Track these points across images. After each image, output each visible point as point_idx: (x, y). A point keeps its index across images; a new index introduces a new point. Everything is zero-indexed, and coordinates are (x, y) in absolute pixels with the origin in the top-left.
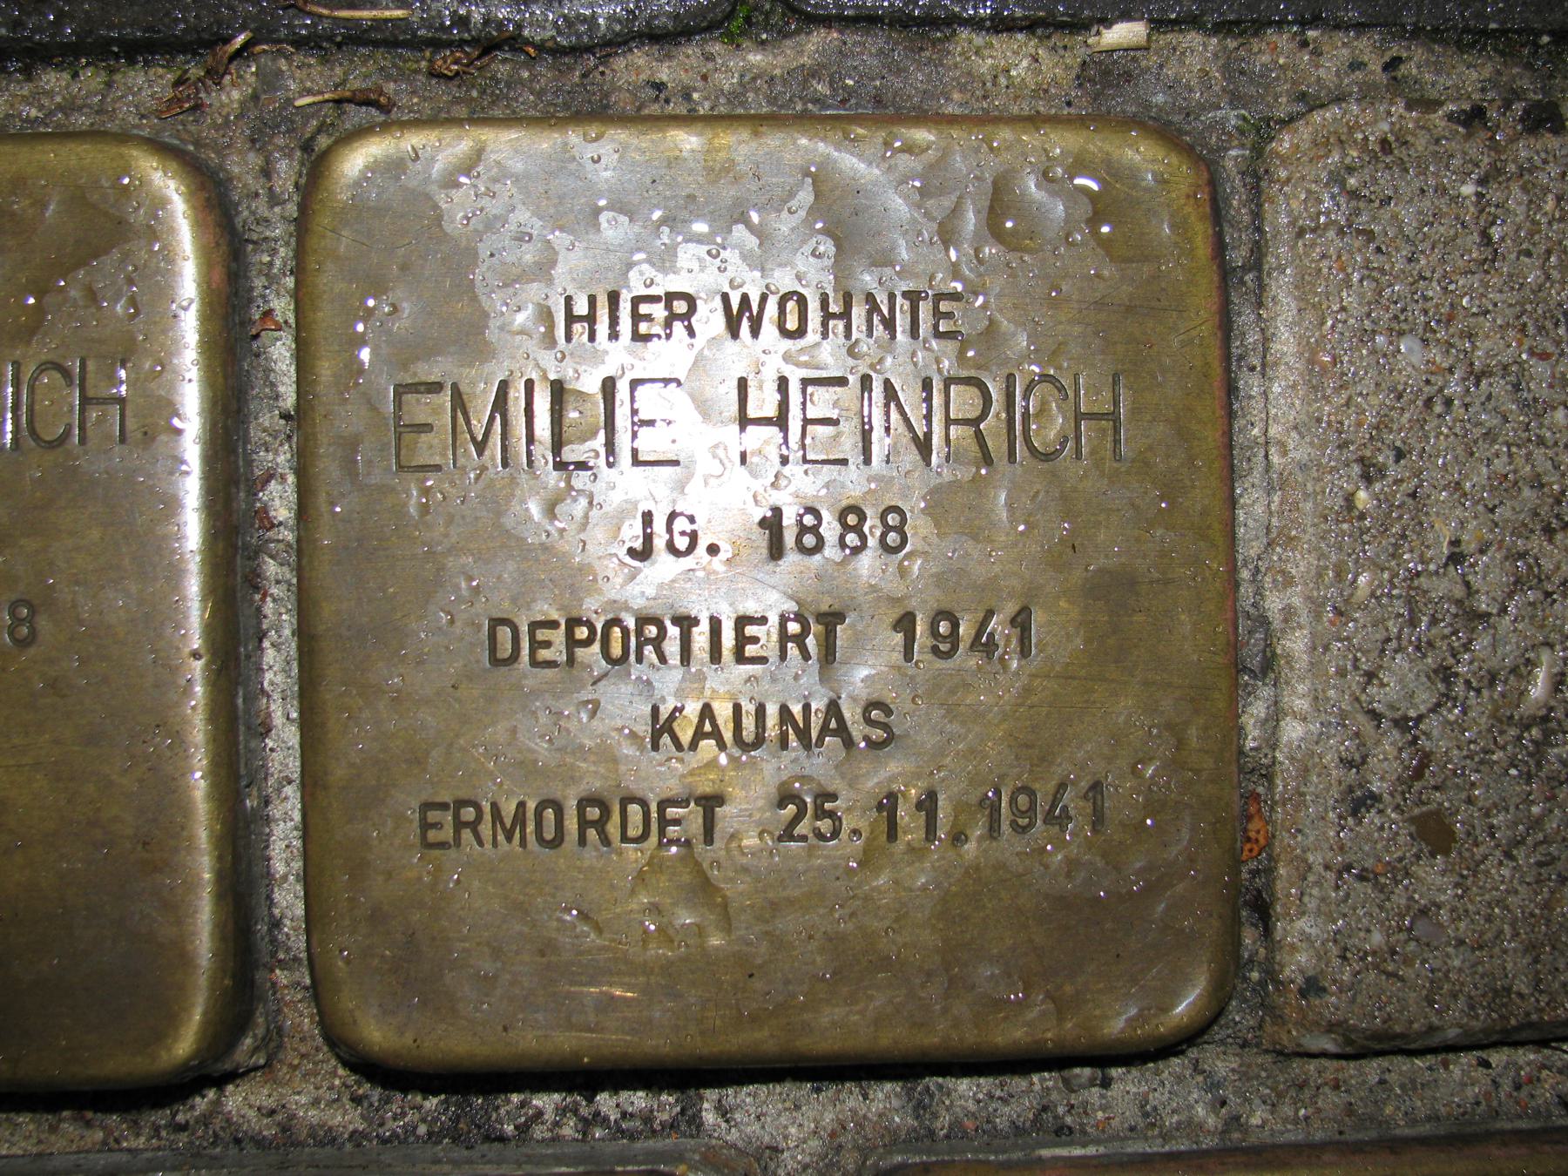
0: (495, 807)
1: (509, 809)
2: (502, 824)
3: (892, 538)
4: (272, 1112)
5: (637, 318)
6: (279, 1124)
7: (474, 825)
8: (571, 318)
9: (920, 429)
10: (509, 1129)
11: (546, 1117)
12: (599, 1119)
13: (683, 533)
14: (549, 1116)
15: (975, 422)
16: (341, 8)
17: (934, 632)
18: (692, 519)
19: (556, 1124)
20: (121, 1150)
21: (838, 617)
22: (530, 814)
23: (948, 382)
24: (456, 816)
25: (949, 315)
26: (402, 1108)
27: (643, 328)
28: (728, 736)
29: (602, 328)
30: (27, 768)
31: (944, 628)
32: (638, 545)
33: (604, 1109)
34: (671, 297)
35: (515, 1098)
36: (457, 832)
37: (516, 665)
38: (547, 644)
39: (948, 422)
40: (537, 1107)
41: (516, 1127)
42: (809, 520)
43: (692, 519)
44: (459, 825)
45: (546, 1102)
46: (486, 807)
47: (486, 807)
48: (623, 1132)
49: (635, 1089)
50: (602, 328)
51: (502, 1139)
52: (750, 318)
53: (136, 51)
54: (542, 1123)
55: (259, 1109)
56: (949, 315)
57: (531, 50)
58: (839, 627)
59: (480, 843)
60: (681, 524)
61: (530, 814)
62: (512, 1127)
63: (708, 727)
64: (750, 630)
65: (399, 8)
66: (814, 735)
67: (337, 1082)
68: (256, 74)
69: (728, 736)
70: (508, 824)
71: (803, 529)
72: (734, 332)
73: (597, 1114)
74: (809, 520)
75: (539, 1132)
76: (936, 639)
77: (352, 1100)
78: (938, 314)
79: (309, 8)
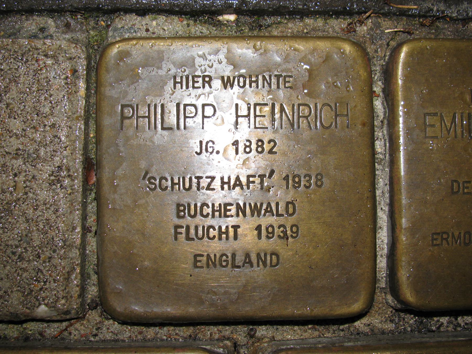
0: (453, 233)
1: (456, 234)
2: (455, 238)
3: (260, 149)
4: (369, 325)
5: (194, 82)
6: (370, 328)
7: (446, 239)
8: (175, 83)
9: (290, 117)
10: (434, 328)
11: (444, 325)
12: (459, 325)
13: (210, 147)
14: (445, 324)
15: (306, 117)
16: (398, 5)
17: (294, 181)
18: (213, 143)
19: (447, 327)
20: (325, 337)
21: (239, 227)
22: (462, 235)
23: (299, 105)
24: (442, 236)
25: (289, 82)
26: (403, 323)
27: (196, 85)
28: (275, 212)
29: (184, 83)
30: (322, 223)
31: (297, 180)
32: (199, 151)
33: (460, 322)
34: (204, 77)
35: (435, 319)
36: (442, 241)
37: (192, 190)
38: (198, 82)
39: (299, 117)
40: (441, 322)
41: (436, 328)
42: (248, 144)
43: (213, 143)
44: (442, 239)
45: (444, 320)
46: (450, 234)
47: (450, 234)
48: (465, 328)
49: (468, 316)
50: (184, 83)
51: (434, 331)
52: (230, 84)
53: (337, 14)
54: (443, 327)
55: (364, 324)
56: (289, 82)
57: (448, 19)
58: (264, 178)
59: (448, 244)
60: (210, 144)
61: (462, 235)
62: (434, 328)
63: (238, 183)
64: (179, 230)
65: (414, 5)
66: (263, 212)
67: (387, 316)
68: (372, 22)
69: (275, 212)
70: (456, 238)
71: (246, 146)
72: (225, 88)
73: (458, 323)
74: (248, 144)
75: (442, 329)
76: (294, 183)
77: (390, 321)
78: (285, 82)
79: (392, 4)
